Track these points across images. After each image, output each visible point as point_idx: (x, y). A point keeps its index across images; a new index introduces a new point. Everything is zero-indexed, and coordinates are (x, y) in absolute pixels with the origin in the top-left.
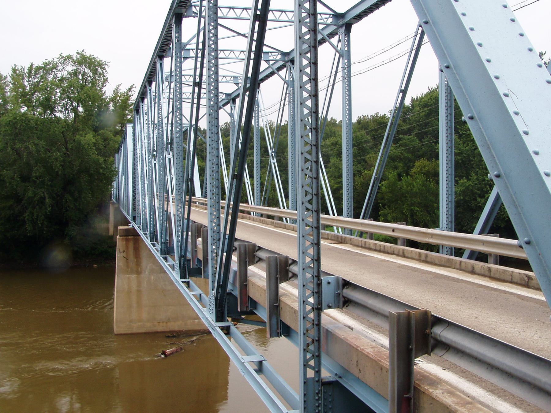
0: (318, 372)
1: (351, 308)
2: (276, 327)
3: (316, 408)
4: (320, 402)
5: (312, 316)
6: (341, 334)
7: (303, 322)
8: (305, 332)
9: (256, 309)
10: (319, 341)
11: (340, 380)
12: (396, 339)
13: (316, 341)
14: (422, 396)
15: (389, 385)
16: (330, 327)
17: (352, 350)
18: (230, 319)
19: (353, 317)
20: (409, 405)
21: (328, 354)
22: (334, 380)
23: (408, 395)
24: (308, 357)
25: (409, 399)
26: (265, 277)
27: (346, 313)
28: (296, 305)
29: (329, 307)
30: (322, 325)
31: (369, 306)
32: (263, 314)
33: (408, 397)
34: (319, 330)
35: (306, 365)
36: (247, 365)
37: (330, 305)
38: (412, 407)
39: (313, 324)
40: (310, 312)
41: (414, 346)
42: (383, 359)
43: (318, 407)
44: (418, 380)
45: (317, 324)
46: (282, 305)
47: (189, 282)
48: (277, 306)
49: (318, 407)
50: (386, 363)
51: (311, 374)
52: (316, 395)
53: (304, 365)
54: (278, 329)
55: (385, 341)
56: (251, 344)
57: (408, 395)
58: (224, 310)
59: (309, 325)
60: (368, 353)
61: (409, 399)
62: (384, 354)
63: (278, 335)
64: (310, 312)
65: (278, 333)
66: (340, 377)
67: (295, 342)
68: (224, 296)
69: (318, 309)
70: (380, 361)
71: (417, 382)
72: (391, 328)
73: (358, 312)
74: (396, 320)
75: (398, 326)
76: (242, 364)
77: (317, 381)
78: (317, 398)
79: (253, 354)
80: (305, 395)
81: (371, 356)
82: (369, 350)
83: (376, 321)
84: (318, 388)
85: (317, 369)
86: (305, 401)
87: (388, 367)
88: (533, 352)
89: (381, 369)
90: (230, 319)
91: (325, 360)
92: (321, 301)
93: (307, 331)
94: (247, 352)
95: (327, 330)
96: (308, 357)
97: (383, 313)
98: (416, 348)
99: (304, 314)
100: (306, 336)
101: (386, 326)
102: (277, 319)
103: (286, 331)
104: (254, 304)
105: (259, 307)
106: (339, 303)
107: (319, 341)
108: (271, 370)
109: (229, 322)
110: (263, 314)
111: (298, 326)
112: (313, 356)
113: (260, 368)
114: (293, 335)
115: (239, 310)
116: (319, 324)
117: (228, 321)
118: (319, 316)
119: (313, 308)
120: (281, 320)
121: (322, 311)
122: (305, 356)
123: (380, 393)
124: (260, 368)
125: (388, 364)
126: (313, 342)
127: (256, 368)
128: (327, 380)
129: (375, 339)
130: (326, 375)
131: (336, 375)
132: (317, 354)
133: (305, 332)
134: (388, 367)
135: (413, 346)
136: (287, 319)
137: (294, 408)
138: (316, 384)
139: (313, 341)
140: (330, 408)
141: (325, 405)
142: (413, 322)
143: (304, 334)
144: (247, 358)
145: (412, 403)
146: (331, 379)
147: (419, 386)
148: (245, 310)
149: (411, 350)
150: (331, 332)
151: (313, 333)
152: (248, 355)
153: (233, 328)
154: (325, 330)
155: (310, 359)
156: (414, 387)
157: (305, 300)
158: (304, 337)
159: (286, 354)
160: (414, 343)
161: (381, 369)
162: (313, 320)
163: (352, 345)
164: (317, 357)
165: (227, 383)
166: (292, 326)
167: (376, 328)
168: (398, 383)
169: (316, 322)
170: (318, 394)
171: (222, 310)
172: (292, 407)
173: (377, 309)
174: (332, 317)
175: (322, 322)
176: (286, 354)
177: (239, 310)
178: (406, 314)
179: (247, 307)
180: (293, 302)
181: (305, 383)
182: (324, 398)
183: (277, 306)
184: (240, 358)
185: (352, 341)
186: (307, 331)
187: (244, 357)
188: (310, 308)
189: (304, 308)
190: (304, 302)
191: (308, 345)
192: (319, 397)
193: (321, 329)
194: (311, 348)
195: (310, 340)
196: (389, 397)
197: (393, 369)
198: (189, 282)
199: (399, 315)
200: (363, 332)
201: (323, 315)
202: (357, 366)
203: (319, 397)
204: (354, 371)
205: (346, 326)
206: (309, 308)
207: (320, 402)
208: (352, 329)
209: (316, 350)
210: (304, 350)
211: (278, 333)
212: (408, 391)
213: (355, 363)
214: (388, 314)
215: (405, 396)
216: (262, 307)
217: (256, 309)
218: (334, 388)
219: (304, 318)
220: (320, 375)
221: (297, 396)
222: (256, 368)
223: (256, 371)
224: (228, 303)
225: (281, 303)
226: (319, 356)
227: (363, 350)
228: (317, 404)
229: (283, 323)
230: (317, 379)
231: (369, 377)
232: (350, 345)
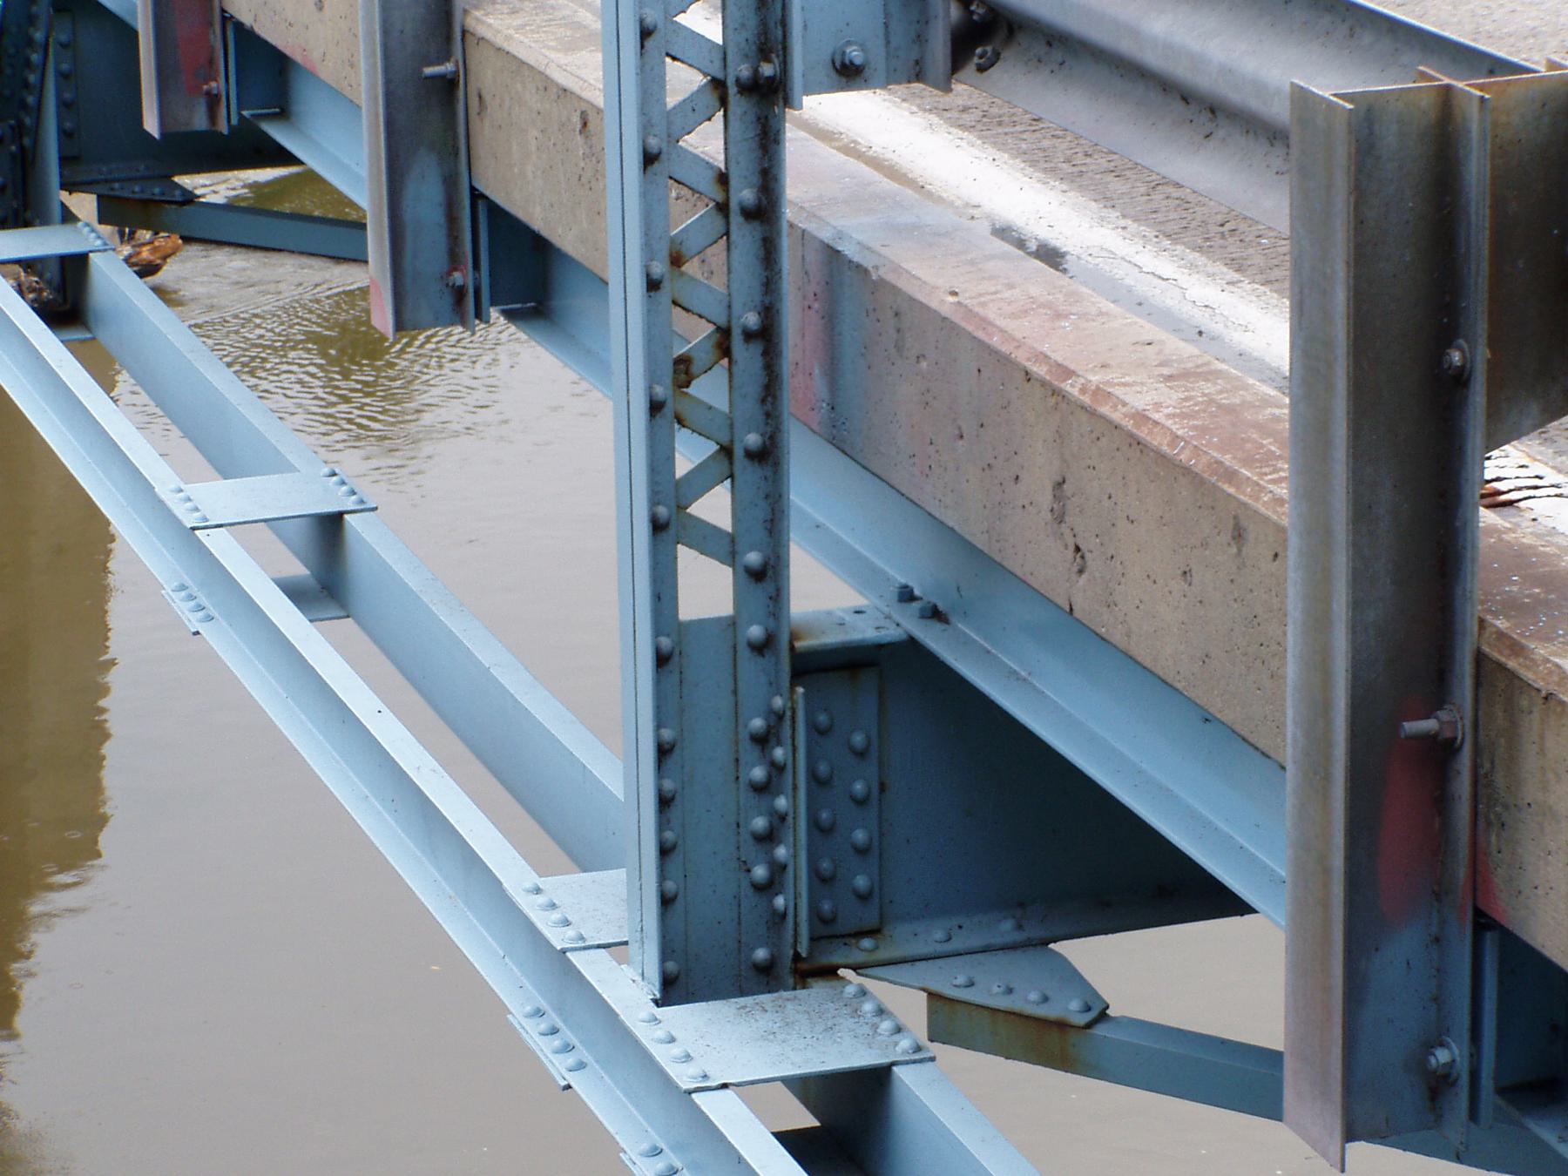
0: (765, 578)
1: (1014, 84)
2: (442, 261)
3: (750, 850)
4: (782, 803)
5: (708, 142)
6: (931, 279)
7: (644, 194)
8: (659, 268)
9: (283, 112)
10: (774, 351)
11: (933, 639)
12: (1340, 298)
13: (749, 336)
14: (1532, 724)
15: (1292, 646)
16: (855, 233)
17: (1012, 394)
18: (84, 205)
19: (1042, 162)
20: (1441, 801)
21: (839, 435)
22: (891, 634)
23: (1428, 725)
24: (683, 465)
25: (1440, 751)
26: (1285, 365)
27: (985, 127)
28: (586, 71)
29: (848, 74)
30: (788, 213)
31: (1152, 59)
32: (341, 151)
33: (1429, 739)
34: (769, 253)
35: (667, 527)
36: (218, 543)
37: (855, 55)
38: (1463, 811)
39: (723, 208)
40: (692, 113)
41: (1483, 354)
42: (1248, 462)
43: (768, 839)
44: (1512, 607)
45: (754, 204)
46: (485, 76)
47: (74, 268)
48: (449, 85)
49: (768, 839)
50: (1273, 489)
51: (707, 590)
52: (749, 752)
53: (658, 527)
54: (454, 261)
55: (1259, 327)
56: (269, 413)
57: (1428, 725)
58: (37, 131)
59: (688, 216)
60: (1141, 417)
61: (1440, 751)
62: (1261, 427)
63: (463, 307)
64: (692, 113)
65: (459, 294)
66: (935, 614)
67: (592, 361)
68: (31, 20)
69: (758, 91)
70: (1231, 476)
71: (1501, 624)
72: (1308, 216)
73: (1067, 105)
74: (1342, 152)
75: (1360, 194)
76: (187, 539)
77: (761, 648)
78: (758, 773)
79: (275, 464)
80: (663, 752)
81: (1160, 442)
82: (1144, 397)
83: (1211, 174)
84: (765, 692)
85: (753, 558)
86: (664, 802)
87: (1284, 516)
88: (1433, 23)
89: (1239, 535)
90: (84, 205)
91: (813, 484)
92: (784, 23)
93: (676, 261)
94: (225, 455)
95: (832, 255)
96: (683, 465)
97: (1254, 104)
98: (1492, 365)
99: (646, 127)
100: (664, 296)
101: (1265, 200)
102: (450, 183)
103: (521, 275)
104: (270, 73)
105: (307, 101)
106: (920, 39)
107: (766, 335)
108: (412, 581)
109: (80, 228)
110: (341, 151)
111: (602, 224)
112: (726, 451)
113: (326, 564)
114: (572, 299)
115: (151, 124)
116: (765, 212)
117: (68, 217)
118: (768, 141)
119: (718, 84)
120: (476, 196)
121: (788, 102)
122: (660, 460)
123: (1216, 706)
124: (326, 564)
125: (1283, 491)
126: (724, 349)
127: (297, 569)
128: (832, 638)
129: (1201, 318)
130: (827, 596)
131: (907, 595)
132: (753, 439)
133: (659, 268)
134: (1284, 516)
135: (1472, 353)
136: (524, 178)
137: (584, 857)
138: (750, 666)
139: (723, 342)
140: (862, 851)
141: (820, 830)
142: (1476, 171)
143: (653, 285)
144: (220, 498)
145: (1463, 785)
146: (866, 631)
147: (1517, 649)
148: (200, 122)
149: (1460, 379)
150: (860, 269)
151: (719, 276)
152: (227, 469)
153: (111, 275)
154: (813, 257)
155: (700, 482)
156: (1480, 658)
157: (653, 16)
158: (650, 313)
159: (531, 451)
160: (1481, 327)
161: (1239, 535)
162: (723, 179)
163: (1020, 356)
164: (759, 461)
165: (93, 733)
166: (564, 237)
167: (1214, 236)
168: (1355, 628)
169: (744, 194)
170: (762, 741)
171: (19, 130)
172: (217, 469)
173: (1203, 81)
174: (876, 163)
175: (796, 191)
176: (531, 451)
177: (151, 124)
178: (1426, 102)
179: (213, 101)
180: (569, 47)
181: (662, 660)
182: (813, 776)
183: (449, 85)
184: (530, 906)
185: (1020, 328)
186: (676, 261)
187: (197, 490)
188: (698, 80)
189: (651, 85)
190: (645, 33)
191: (684, 370)
192: (777, 769)
193: (786, 244)
194: (710, 389)
195: (695, 334)
196: (1290, 743)
197: (1317, 530)
198: (74, 268)
199: (1367, 118)
200: (1119, 271)
201: (796, 144)
202: (1060, 519)
203: (777, 769)
204: (1038, 557)
205: (1003, 232)
206: (683, 81)
207: (782, 803)
208: (1051, 256)
209: (750, 407)
210: (655, 407)
211: (459, 294)
212: (1437, 691)
213: (1046, 499)
214: (1279, 111)
215: (429, 71)
216: (336, 94)
217: (283, 112)
218: (889, 681)
219: (649, 159)
220: (777, 599)
221: (610, 766)
222: (297, 569)
223: (296, 593)
224: (63, 76)
225: (476, 56)
226: (768, 456)
227: (1100, 393)
228: (760, 823)
229: (239, 27)
230: (756, 632)
231: (1151, 603)
232: (1003, 360)
